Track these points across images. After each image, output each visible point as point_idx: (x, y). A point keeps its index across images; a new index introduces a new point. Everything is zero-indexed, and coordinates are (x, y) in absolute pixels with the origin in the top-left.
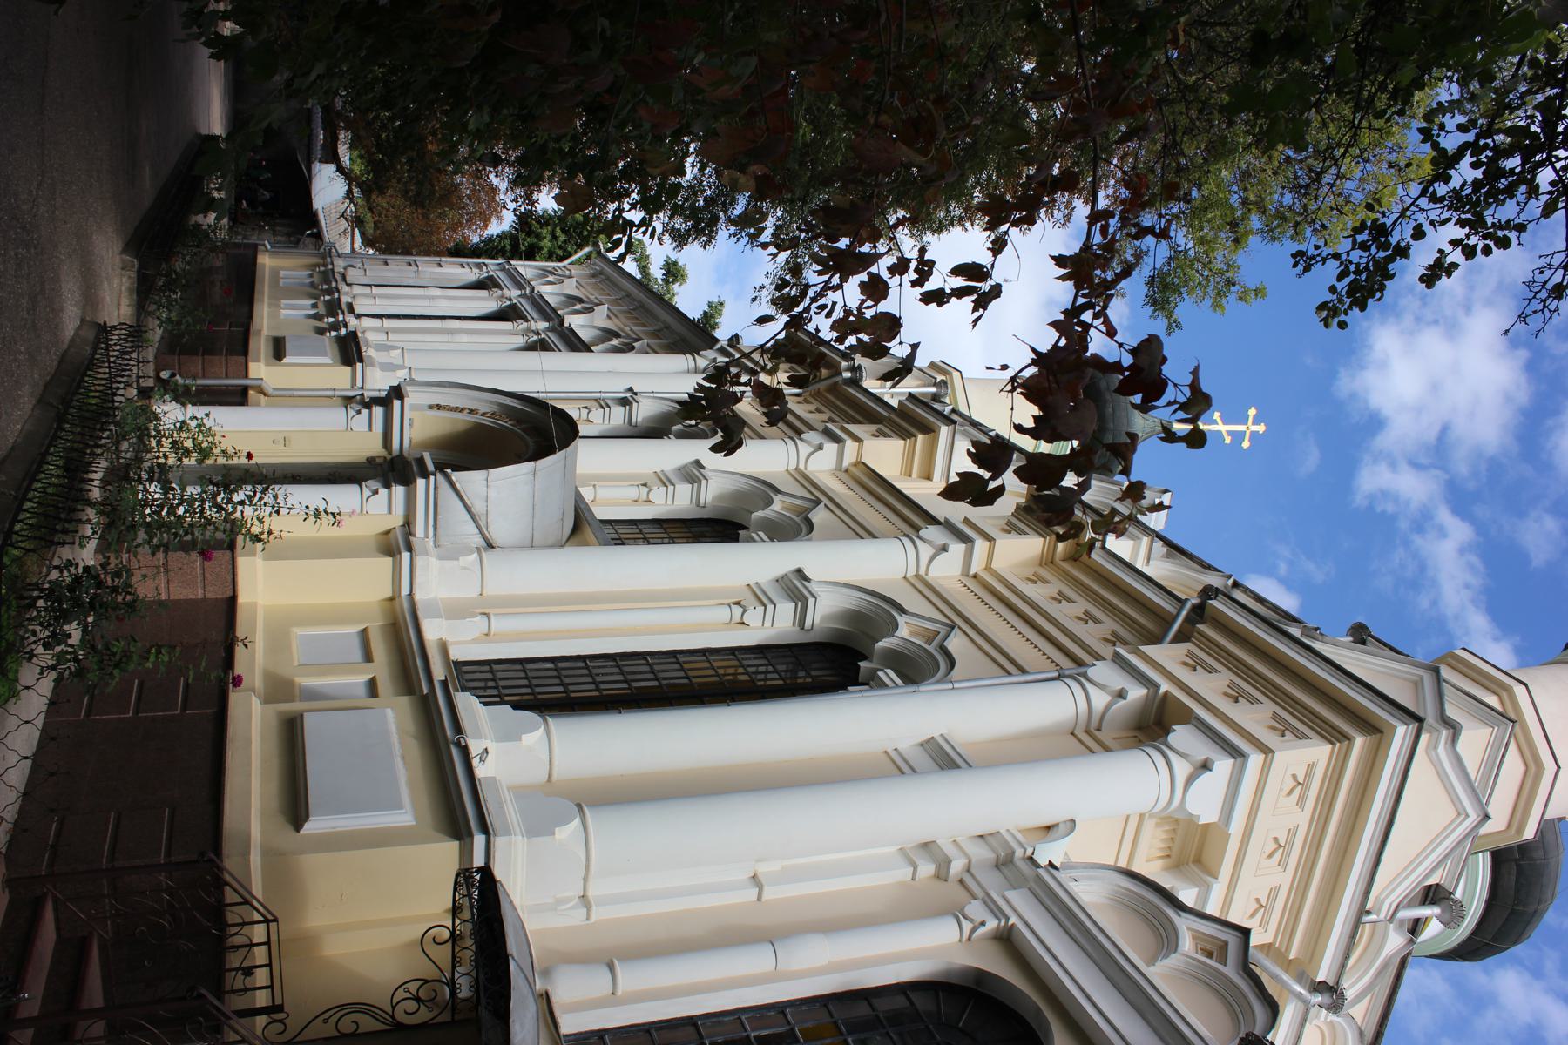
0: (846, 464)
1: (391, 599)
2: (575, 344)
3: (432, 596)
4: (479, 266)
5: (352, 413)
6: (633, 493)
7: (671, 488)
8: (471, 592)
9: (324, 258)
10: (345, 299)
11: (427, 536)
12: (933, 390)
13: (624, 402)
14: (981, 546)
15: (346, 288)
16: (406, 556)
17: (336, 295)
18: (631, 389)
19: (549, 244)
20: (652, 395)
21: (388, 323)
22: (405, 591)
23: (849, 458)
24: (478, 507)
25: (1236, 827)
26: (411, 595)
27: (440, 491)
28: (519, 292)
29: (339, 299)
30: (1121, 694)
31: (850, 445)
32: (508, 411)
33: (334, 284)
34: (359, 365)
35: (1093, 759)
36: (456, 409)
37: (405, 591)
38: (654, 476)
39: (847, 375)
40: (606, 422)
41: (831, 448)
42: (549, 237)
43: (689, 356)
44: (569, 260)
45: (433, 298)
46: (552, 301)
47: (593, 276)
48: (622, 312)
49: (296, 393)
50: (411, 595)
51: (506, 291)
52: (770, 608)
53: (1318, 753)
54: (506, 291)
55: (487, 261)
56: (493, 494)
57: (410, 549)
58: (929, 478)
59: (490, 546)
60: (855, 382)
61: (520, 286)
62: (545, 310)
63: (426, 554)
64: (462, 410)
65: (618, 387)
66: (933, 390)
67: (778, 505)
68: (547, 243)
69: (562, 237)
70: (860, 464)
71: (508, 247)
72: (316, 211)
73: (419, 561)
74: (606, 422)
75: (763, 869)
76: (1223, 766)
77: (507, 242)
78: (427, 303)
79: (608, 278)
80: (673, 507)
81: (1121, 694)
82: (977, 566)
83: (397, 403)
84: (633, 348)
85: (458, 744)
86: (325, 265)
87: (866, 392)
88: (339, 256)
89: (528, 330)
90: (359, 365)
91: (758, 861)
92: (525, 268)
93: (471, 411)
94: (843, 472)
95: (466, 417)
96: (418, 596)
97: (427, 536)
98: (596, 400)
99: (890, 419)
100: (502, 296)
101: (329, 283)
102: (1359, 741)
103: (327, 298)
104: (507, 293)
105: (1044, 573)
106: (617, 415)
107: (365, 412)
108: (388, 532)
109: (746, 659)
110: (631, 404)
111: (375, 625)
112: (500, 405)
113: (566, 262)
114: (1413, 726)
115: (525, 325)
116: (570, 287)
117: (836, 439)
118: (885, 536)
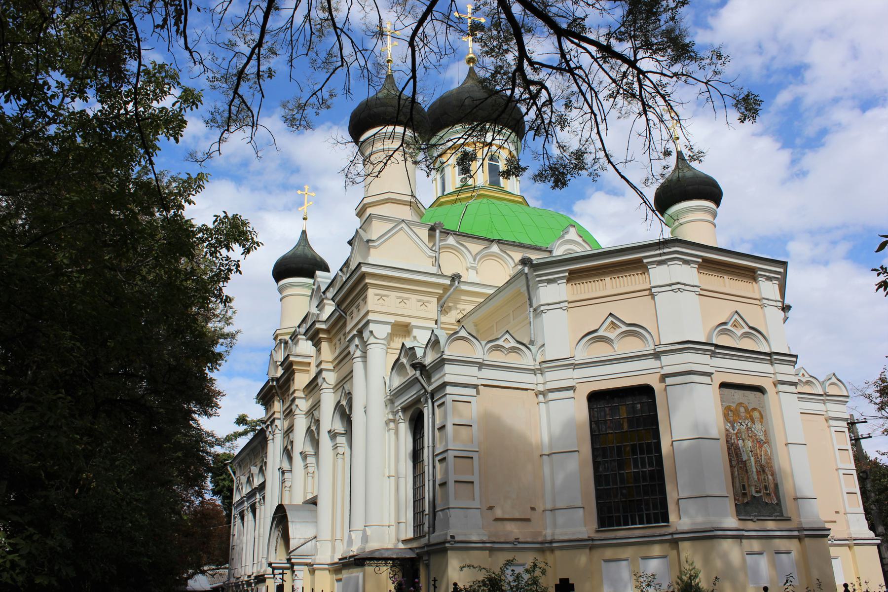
0: (303, 396)
1: (329, 571)
2: (262, 486)
3: (329, 557)
4: (235, 518)
5: (296, 578)
6: (340, 461)
7: (308, 465)
8: (329, 544)
9: (230, 587)
10: (246, 579)
11: (311, 558)
12: (283, 344)
13: (283, 473)
14: (323, 366)
15: (242, 578)
16: (315, 566)
17: (244, 582)
18: (279, 469)
19: (227, 482)
20: (281, 461)
21: (255, 562)
22: (327, 566)
23: (302, 395)
24: (302, 541)
25: (392, 319)
26: (328, 565)
27: (295, 554)
28: (246, 503)
29: (246, 581)
30: (357, 346)
31: (297, 394)
32: (277, 526)
33: (240, 583)
34: (266, 576)
35: (294, 430)
36: (277, 544)
37: (327, 566)
38: (335, 450)
39: (275, 383)
40: (344, 445)
41: (297, 402)
42: (224, 482)
43: (268, 442)
44: (234, 477)
45: (259, 535)
46: (249, 490)
47: (240, 467)
48: (254, 459)
49: (398, 395)
50: (328, 565)
51: (245, 508)
52: (338, 445)
53: (371, 292)
54: (245, 508)
55: (233, 514)
56: (298, 536)
57: (313, 565)
58: (310, 363)
59: (315, 537)
60: (278, 380)
61: (243, 502)
62: (251, 495)
63: (315, 559)
64: (277, 542)
65: (278, 474)
66: (283, 344)
67: (344, 403)
68: (226, 483)
69: (224, 476)
70: (304, 390)
71: (228, 501)
72: (211, 588)
73: (317, 562)
74: (344, 445)
75: (387, 474)
76: (372, 327)
77: (226, 501)
78: (248, 544)
79: (241, 461)
80: (346, 444)
81: (357, 346)
82: (331, 367)
83: (273, 565)
84: (350, 393)
85: (349, 558)
86: (232, 586)
87: (282, 376)
88: (229, 580)
89: (259, 502)
90: (266, 576)
91: (384, 476)
92: (236, 498)
93: (277, 538)
94: (306, 398)
95: (279, 540)
96: (329, 562)
97: (311, 558)
98: (282, 483)
99: (289, 375)
100: (247, 510)
101: (240, 585)
102: (367, 281)
103: (245, 586)
104: (245, 508)
105: (334, 342)
106: (311, 460)
107: (296, 573)
108: (310, 571)
109: (428, 409)
110: (284, 471)
111: (335, 577)
112: (275, 528)
113: (234, 478)
114: (362, 265)
115: (257, 503)
116: (244, 479)
117: (274, 420)
118: (320, 397)
